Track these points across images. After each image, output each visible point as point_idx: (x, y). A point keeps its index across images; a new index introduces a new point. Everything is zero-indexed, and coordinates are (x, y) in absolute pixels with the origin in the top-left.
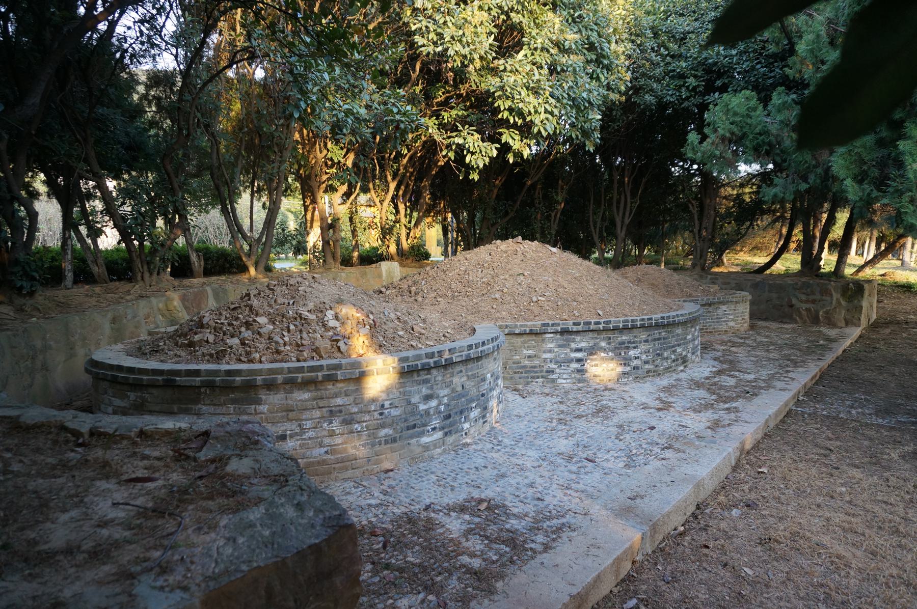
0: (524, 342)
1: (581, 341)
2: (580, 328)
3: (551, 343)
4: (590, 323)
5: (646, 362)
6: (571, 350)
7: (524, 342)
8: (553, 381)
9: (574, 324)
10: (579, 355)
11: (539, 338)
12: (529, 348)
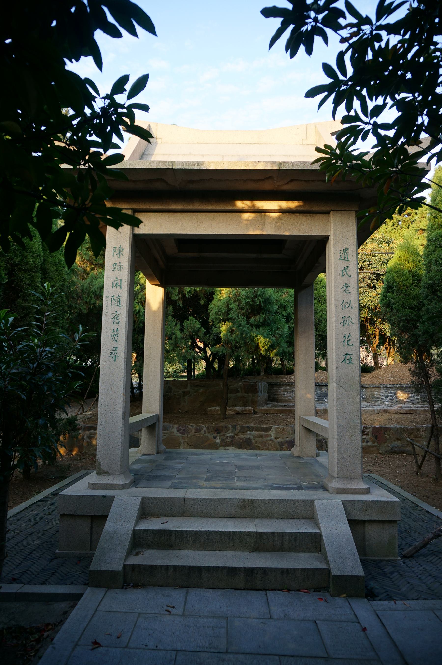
0: (375, 390)
1: (392, 390)
2: (390, 386)
3: (383, 390)
4: (394, 385)
5: (417, 399)
6: (389, 393)
7: (375, 390)
8: (383, 402)
9: (389, 385)
10: (391, 394)
11: (379, 389)
12: (376, 391)
